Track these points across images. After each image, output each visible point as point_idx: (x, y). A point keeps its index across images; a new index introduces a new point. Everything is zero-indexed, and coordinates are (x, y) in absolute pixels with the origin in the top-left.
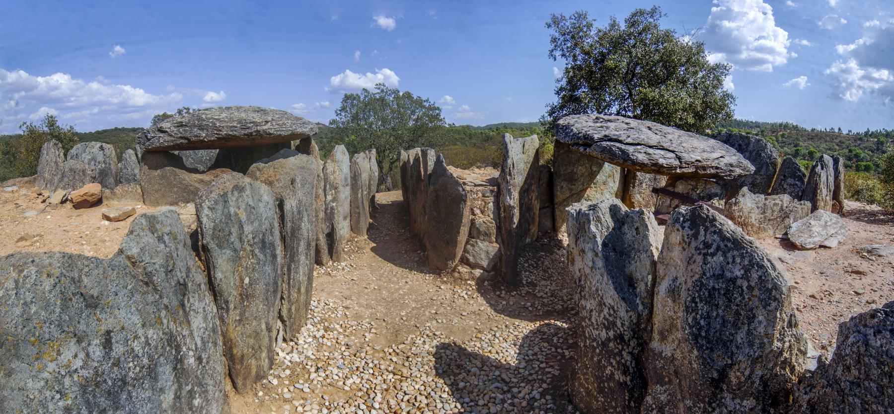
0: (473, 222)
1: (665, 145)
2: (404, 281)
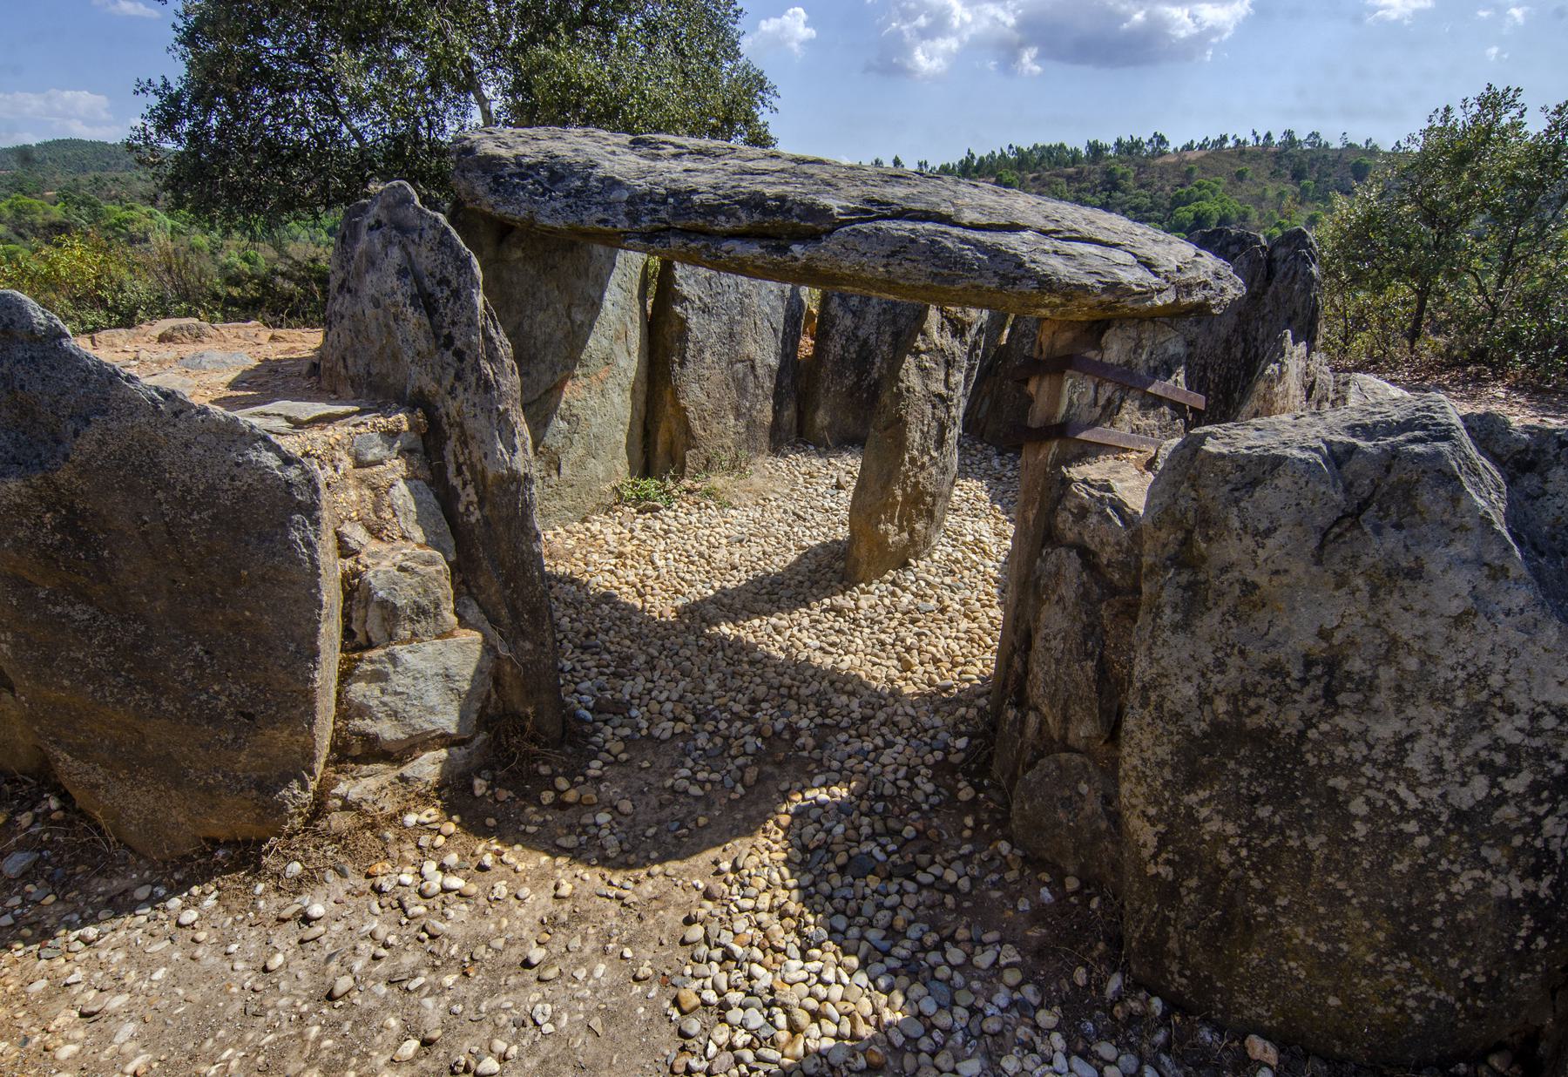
0: (354, 589)
1: (946, 209)
2: (65, 1017)
